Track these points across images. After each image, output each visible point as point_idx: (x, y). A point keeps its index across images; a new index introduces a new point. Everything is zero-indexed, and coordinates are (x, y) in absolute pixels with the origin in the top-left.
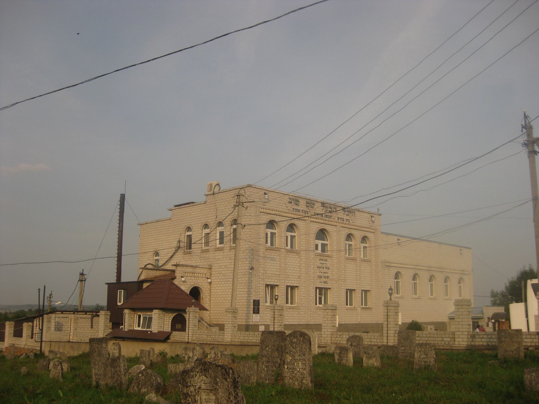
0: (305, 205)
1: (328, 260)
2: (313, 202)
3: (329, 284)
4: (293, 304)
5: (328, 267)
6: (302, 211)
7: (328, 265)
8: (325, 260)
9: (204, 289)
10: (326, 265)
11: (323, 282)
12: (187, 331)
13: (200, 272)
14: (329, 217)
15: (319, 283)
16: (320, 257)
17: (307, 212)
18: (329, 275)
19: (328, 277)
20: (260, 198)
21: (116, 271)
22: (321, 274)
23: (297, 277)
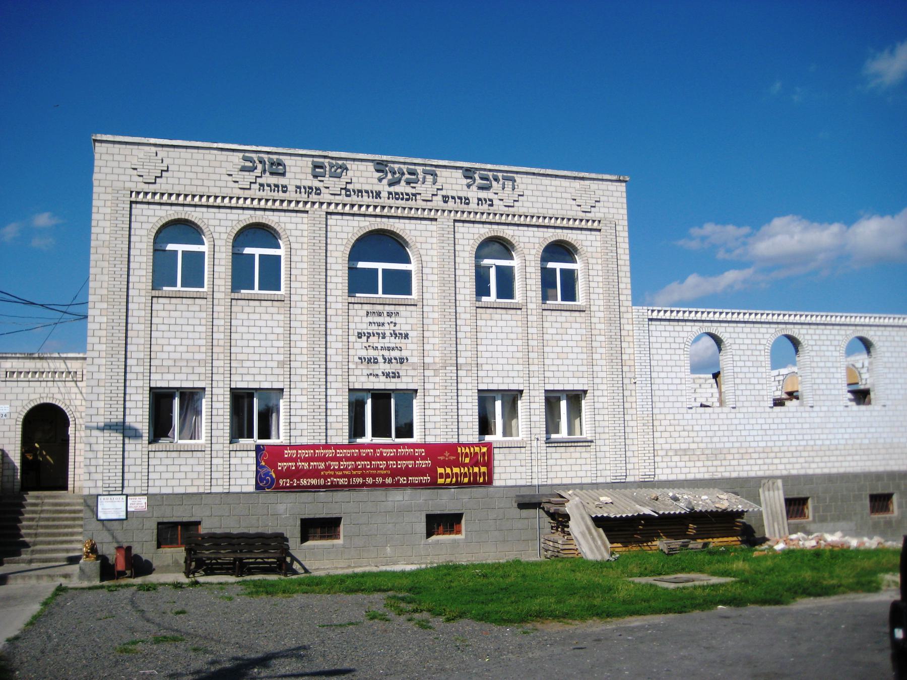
0: (310, 170)
1: (402, 314)
2: (340, 162)
3: (404, 379)
4: (511, 435)
5: (400, 334)
6: (298, 187)
7: (403, 328)
8: (389, 314)
9: (806, 342)
10: (394, 328)
11: (380, 374)
12: (106, 583)
13: (499, 210)
14: (405, 197)
15: (364, 379)
16: (366, 307)
17: (317, 189)
18: (404, 354)
19: (401, 361)
20: (133, 167)
21: (316, 677)
22: (372, 353)
23: (275, 364)
